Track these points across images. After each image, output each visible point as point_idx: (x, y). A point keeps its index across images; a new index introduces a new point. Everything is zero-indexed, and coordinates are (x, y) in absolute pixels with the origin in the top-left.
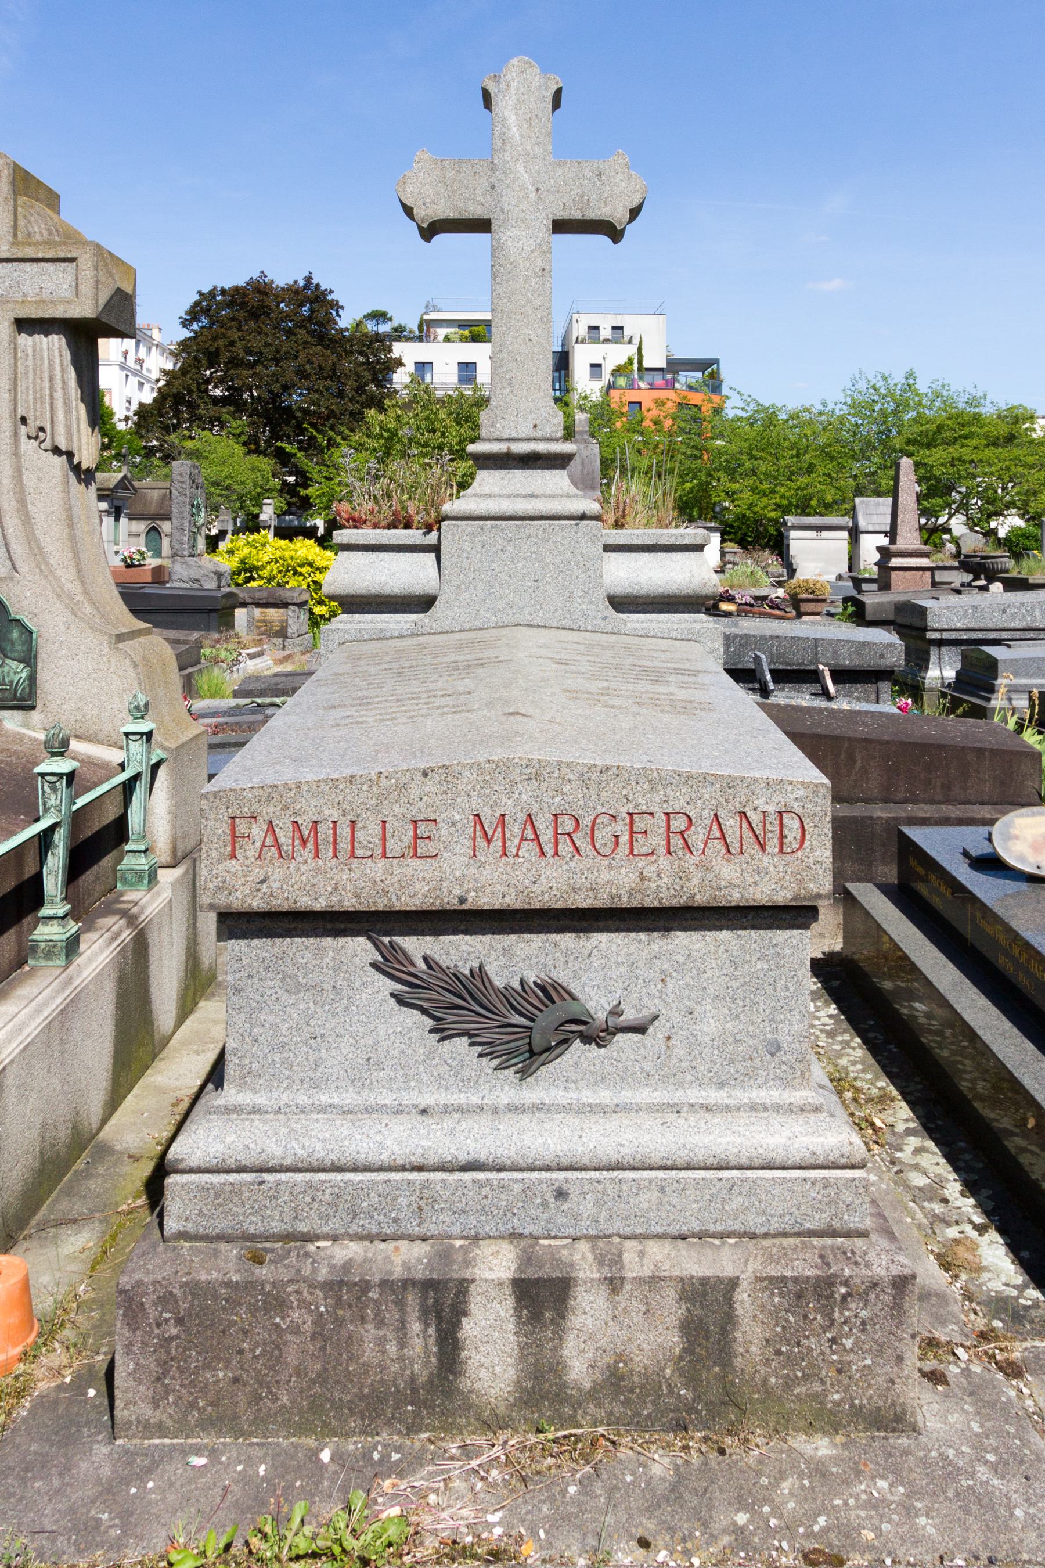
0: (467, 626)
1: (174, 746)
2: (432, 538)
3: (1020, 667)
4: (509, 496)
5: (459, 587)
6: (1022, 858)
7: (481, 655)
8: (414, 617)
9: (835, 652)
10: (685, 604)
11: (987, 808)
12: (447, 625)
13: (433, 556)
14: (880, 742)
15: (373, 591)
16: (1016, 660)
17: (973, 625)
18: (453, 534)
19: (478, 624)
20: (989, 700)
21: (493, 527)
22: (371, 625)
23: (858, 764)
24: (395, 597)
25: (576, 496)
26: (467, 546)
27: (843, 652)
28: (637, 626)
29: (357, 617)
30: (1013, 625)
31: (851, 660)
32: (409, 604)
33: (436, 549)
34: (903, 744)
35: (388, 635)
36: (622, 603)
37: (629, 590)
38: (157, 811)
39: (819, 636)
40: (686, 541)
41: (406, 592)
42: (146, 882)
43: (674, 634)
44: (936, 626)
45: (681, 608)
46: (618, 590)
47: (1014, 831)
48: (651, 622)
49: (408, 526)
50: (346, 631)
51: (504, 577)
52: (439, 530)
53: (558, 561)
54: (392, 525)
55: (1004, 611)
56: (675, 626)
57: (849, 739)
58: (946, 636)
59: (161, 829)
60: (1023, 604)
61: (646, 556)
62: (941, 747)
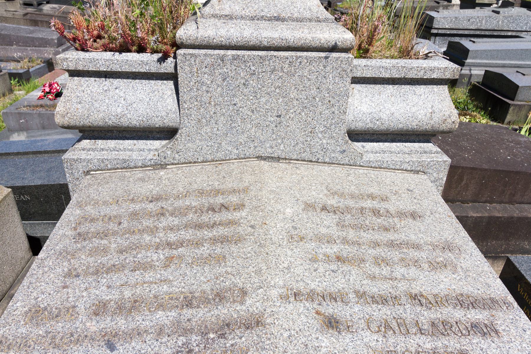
0: (210, 158)
2: (168, 66)
4: (252, 19)
5: (199, 121)
8: (157, 144)
12: (189, 156)
13: (171, 84)
14: (482, 170)
16: (478, 51)
17: (453, 27)
18: (190, 65)
19: (220, 155)
21: (235, 58)
23: (464, 182)
25: (326, 20)
26: (206, 79)
28: (371, 157)
30: (471, 27)
33: (173, 77)
35: (132, 165)
36: (356, 136)
37: (370, 125)
40: (435, 76)
41: (143, 125)
43: (406, 166)
44: (437, 26)
46: (360, 126)
48: (384, 152)
49: (141, 49)
50: (89, 161)
51: (246, 111)
52: (175, 57)
53: (303, 96)
54: (124, 49)
55: (469, 20)
56: (408, 158)
57: (463, 167)
58: (440, 32)
60: (478, 17)
61: (390, 88)
62: (518, 173)
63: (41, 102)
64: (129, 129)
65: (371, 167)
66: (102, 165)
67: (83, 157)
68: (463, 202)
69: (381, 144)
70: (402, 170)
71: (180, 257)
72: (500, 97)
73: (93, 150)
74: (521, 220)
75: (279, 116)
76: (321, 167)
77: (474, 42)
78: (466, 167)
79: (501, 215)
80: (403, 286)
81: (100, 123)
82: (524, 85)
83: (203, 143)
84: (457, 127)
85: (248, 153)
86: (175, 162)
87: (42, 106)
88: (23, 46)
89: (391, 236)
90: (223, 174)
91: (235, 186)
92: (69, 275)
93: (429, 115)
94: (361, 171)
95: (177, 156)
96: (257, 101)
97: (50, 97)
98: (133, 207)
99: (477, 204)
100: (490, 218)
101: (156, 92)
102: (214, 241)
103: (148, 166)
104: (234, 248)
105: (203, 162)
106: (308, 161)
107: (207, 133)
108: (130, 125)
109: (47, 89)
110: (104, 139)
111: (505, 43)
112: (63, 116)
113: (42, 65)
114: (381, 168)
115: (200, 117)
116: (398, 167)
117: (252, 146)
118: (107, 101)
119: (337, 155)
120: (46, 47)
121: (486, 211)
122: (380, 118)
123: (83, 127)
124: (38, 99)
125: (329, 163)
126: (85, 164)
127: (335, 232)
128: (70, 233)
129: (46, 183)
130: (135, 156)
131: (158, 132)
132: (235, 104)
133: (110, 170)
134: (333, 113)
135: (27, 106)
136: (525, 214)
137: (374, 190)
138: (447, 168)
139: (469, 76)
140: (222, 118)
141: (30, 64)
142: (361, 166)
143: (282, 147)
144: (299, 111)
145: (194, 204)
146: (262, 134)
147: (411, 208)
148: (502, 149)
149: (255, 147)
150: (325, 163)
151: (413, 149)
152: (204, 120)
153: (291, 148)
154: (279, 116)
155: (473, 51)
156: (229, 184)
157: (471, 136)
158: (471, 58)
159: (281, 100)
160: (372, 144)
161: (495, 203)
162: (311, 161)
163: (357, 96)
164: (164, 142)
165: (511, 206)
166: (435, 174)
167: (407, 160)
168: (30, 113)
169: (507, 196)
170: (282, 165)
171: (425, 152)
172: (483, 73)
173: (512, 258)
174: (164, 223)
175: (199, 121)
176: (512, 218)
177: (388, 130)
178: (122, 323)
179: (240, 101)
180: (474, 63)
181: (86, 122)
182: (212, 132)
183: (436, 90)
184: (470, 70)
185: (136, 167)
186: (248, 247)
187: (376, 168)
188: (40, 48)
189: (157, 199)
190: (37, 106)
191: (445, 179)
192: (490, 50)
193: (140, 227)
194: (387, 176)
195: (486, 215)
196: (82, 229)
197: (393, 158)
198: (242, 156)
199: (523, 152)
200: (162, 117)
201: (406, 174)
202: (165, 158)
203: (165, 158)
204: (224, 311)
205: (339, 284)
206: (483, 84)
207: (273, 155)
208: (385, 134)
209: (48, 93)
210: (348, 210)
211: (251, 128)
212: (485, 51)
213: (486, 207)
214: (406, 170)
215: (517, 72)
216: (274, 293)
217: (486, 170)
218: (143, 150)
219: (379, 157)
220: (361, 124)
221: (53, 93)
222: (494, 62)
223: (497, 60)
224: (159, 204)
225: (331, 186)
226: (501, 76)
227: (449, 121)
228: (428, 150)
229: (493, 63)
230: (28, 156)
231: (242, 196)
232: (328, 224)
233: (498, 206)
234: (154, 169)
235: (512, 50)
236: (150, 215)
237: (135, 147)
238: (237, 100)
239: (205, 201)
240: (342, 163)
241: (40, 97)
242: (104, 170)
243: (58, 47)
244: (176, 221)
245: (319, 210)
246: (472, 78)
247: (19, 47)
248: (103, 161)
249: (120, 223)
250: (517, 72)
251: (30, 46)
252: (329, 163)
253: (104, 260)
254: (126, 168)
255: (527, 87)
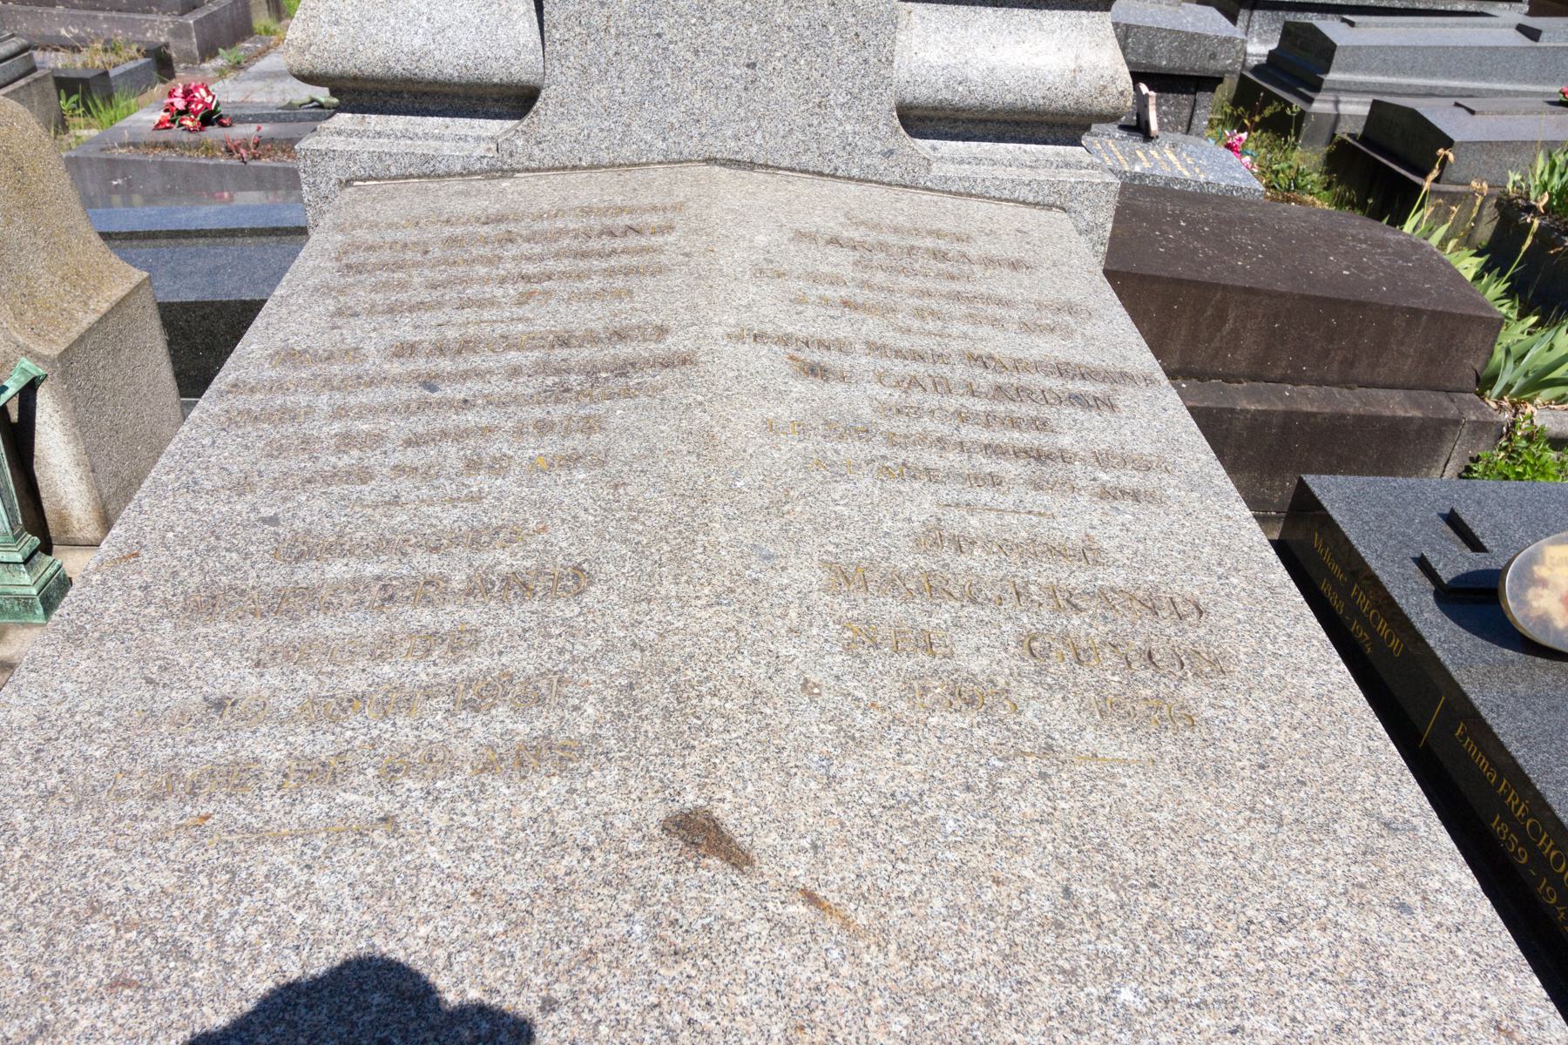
0: (605, 157)
1: (54, 351)
3: (1366, 57)
5: (585, 71)
6: (1545, 621)
7: (631, 312)
8: (494, 127)
9: (1151, 47)
10: (1051, 125)
11: (1399, 395)
14: (1271, 295)
15: (398, 69)
16: (1359, 48)
19: (627, 153)
20: (1310, 101)
22: (403, 145)
23: (1228, 327)
24: (449, 84)
27: (1162, 46)
28: (951, 170)
29: (374, 121)
31: (1170, 60)
32: (481, 99)
34: (1304, 298)
35: (442, 168)
36: (923, 120)
37: (945, 95)
38: (53, 461)
39: (1132, 21)
41: (473, 75)
42: (40, 611)
43: (1023, 193)
45: (1042, 132)
46: (922, 94)
47: (1541, 571)
50: (351, 156)
51: (682, 52)
56: (1028, 175)
57: (1225, 287)
59: (70, 489)
62: (1360, 305)
63: (163, 136)
64: (437, 88)
65: (950, 192)
66: (379, 166)
67: (339, 147)
68: (1227, 378)
69: (974, 144)
70: (1016, 201)
71: (547, 293)
72: (1403, 172)
73: (360, 135)
74: (1363, 421)
75: (752, 66)
76: (840, 185)
77: (1352, 24)
78: (1234, 288)
79: (1315, 410)
80: (956, 345)
81: (378, 70)
82: (1466, 139)
83: (592, 122)
84: (1129, 104)
85: (686, 151)
86: (533, 165)
87: (167, 145)
88: (85, 8)
89: (957, 286)
90: (632, 184)
91: (657, 201)
92: (339, 313)
93: (1068, 76)
94: (927, 196)
95: (536, 151)
96: (705, 29)
97: (188, 123)
98: (448, 231)
99: (1261, 385)
100: (1289, 415)
101: (495, 7)
102: (611, 273)
103: (475, 173)
104: (649, 281)
105: (591, 167)
106: (814, 173)
107: (600, 100)
108: (440, 77)
109: (180, 104)
110: (382, 113)
111: (1437, 30)
112: (302, 51)
113: (142, 61)
114: (971, 195)
115: (585, 62)
116: (1006, 194)
117: (695, 133)
118: (392, 21)
119: (876, 161)
120: (150, 12)
121: (1281, 399)
122: (966, 80)
123: (341, 78)
124: (157, 128)
125: (859, 180)
126: (342, 163)
127: (848, 271)
128: (329, 264)
129: (209, 298)
130: (447, 148)
131: (497, 101)
132: (659, 35)
133: (394, 178)
134: (866, 61)
135: (129, 144)
136: (1374, 410)
137: (948, 225)
138: (1114, 201)
139: (1332, 120)
140: (632, 65)
141: (112, 57)
142: (928, 189)
143: (758, 139)
144: (793, 56)
145: (571, 226)
146: (716, 107)
147: (1013, 253)
148: (1334, 255)
149: (703, 136)
150: (850, 178)
151: (1041, 157)
152: (594, 70)
153: (779, 140)
154: (752, 66)
155: (1345, 48)
156: (645, 200)
157: (1262, 224)
158: (1339, 69)
159: (755, 29)
160: (954, 143)
161: (1303, 382)
162: (821, 174)
163: (918, 29)
164: (509, 124)
165: (1345, 391)
166: (1087, 214)
167: (1026, 179)
168: (140, 162)
169: (1335, 366)
170: (759, 175)
171: (1067, 165)
172: (1364, 110)
173: (1309, 479)
174: (512, 250)
175: (585, 71)
176: (1343, 416)
177: (983, 108)
178: (445, 364)
179: (671, 27)
180: (1349, 83)
181: (348, 66)
182: (610, 97)
183: (1085, 21)
184: (1337, 102)
185: (449, 175)
186: (676, 280)
187: (961, 194)
188: (132, 15)
189: (500, 219)
190: (155, 146)
191: (1109, 226)
192: (1395, 48)
193: (466, 256)
194: (979, 210)
195: (1281, 407)
196: (353, 259)
197: (997, 174)
198: (675, 156)
199: (1386, 263)
200: (506, 59)
201: (1023, 209)
202: (511, 155)
203: (511, 155)
204: (625, 350)
205: (843, 331)
206: (1364, 139)
207: (739, 157)
208: (981, 121)
209: (181, 113)
210: (883, 247)
211: (693, 93)
212: (1380, 48)
213: (1282, 392)
214: (1024, 202)
215: (1457, 105)
216: (718, 331)
217: (1282, 295)
218: (465, 139)
219: (966, 170)
220: (925, 91)
221: (196, 114)
222: (1404, 81)
223: (1411, 76)
224: (503, 226)
225: (857, 212)
226: (1413, 114)
227: (1113, 90)
228: (1073, 160)
229: (1400, 86)
230: (158, 242)
231: (670, 216)
232: (840, 261)
233: (1312, 391)
234: (487, 178)
235: (1455, 47)
236: (486, 241)
237: (448, 132)
238: (664, 24)
239: (595, 223)
240: (886, 180)
241: (161, 123)
242: (383, 179)
243: (182, 14)
244: (538, 249)
245: (821, 243)
246: (1341, 124)
247: (73, 12)
248: (379, 158)
249: (426, 252)
250: (1457, 105)
251: (102, 9)
252: (859, 180)
253: (403, 297)
254: (428, 176)
255: (1475, 143)
